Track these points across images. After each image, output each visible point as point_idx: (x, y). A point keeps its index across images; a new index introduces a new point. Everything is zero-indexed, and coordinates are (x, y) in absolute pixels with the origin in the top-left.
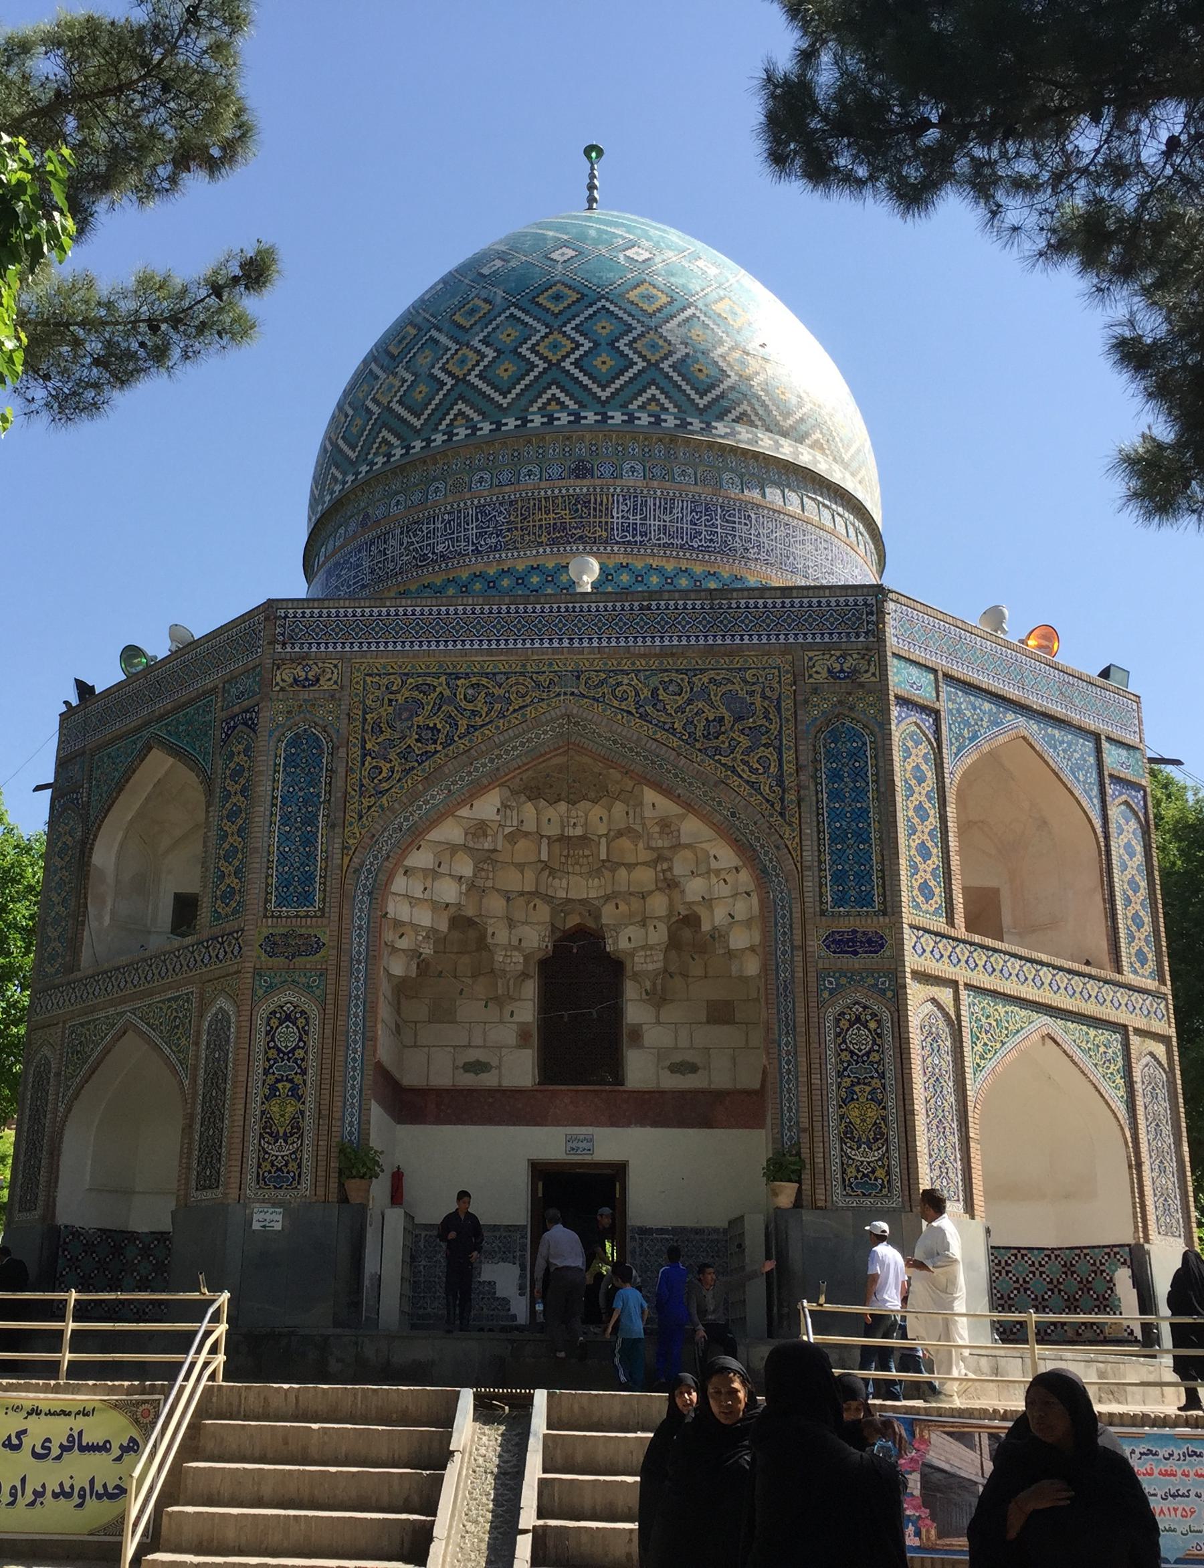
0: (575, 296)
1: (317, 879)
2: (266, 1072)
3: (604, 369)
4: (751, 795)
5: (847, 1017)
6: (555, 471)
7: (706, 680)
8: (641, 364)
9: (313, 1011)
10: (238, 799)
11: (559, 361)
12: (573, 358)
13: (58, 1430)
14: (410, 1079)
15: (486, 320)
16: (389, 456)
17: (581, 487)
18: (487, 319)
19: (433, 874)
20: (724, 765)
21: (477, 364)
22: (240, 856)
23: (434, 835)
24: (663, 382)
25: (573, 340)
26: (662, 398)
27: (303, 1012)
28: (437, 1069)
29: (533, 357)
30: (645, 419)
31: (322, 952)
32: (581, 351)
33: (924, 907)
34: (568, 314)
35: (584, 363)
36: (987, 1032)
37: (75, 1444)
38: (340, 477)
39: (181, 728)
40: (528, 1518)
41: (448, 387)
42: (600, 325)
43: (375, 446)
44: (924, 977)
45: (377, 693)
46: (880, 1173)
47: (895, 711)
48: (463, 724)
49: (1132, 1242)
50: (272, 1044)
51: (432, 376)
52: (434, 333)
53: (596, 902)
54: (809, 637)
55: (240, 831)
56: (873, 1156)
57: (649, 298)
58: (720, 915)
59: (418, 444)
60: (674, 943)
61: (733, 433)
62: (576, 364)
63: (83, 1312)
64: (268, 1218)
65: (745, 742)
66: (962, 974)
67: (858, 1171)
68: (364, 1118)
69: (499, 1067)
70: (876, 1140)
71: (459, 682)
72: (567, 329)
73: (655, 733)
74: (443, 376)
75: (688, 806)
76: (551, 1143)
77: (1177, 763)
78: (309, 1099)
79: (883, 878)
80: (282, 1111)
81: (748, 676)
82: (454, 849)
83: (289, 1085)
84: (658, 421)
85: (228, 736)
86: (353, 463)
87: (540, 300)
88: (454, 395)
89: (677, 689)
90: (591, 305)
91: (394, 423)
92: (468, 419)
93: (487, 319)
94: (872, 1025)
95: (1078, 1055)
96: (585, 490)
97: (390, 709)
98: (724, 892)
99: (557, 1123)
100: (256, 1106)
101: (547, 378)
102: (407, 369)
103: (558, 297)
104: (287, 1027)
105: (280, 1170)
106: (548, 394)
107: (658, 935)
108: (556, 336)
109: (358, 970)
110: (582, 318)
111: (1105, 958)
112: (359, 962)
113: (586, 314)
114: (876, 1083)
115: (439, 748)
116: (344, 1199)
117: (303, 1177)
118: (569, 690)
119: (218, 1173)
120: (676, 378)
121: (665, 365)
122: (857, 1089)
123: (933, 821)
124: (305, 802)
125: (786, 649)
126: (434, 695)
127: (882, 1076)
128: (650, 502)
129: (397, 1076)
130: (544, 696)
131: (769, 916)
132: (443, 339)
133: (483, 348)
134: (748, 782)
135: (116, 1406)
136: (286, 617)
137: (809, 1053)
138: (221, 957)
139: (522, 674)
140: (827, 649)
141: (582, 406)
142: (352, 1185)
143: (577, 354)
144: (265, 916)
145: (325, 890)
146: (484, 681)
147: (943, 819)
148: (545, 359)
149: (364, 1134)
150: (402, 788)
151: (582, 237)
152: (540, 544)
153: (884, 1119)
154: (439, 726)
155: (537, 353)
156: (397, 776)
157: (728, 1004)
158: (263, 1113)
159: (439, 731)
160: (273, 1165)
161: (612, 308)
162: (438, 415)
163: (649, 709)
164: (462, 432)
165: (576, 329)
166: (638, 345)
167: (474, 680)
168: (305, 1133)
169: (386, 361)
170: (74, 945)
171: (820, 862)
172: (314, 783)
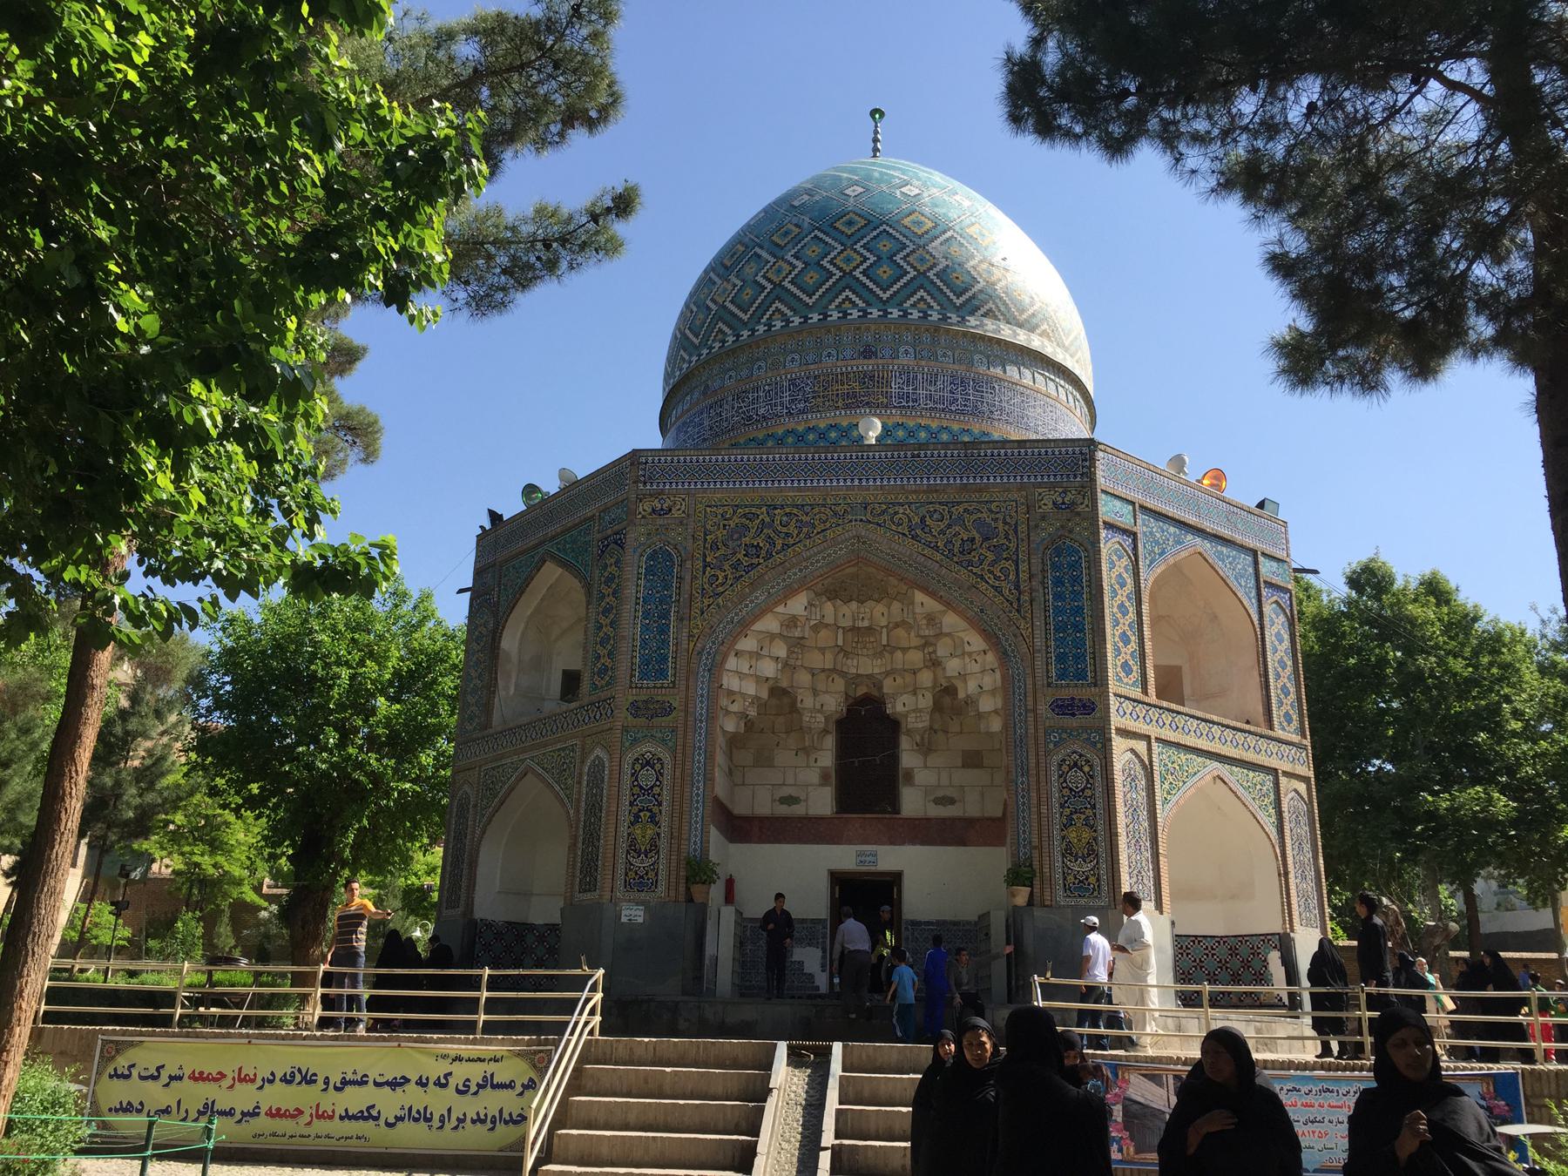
0: (863, 222)
2: (631, 804)
6: (848, 353)
8: (913, 273)
9: (667, 758)
13: (476, 1072)
14: (740, 809)
16: (724, 342)
17: (867, 365)
18: (797, 240)
19: (757, 655)
23: (758, 626)
26: (928, 298)
28: (759, 802)
29: (831, 268)
30: (915, 315)
34: (858, 235)
37: (488, 1083)
40: (828, 1139)
44: (1125, 733)
46: (1092, 880)
47: (1103, 533)
48: (779, 543)
51: (756, 282)
52: (757, 250)
56: (1087, 867)
57: (919, 223)
58: (972, 686)
59: (746, 333)
60: (937, 707)
61: (982, 325)
62: (864, 273)
63: (494, 984)
64: (633, 913)
65: (991, 556)
66: (1154, 731)
72: (857, 246)
74: (764, 282)
75: (948, 605)
76: (846, 857)
77: (1315, 572)
78: (664, 824)
80: (644, 833)
82: (772, 637)
84: (926, 316)
86: (696, 347)
87: (837, 225)
88: (772, 296)
91: (728, 317)
93: (797, 240)
94: (1086, 769)
95: (1241, 791)
98: (974, 668)
99: (850, 842)
100: (624, 830)
101: (842, 284)
103: (850, 223)
107: (926, 701)
111: (1261, 719)
114: (1089, 812)
116: (690, 899)
121: (931, 274)
123: (1132, 616)
124: (661, 602)
125: (1022, 487)
127: (1094, 807)
129: (730, 806)
131: (1009, 686)
132: (764, 254)
133: (795, 262)
135: (519, 1054)
137: (1038, 790)
140: (1052, 486)
142: (696, 889)
147: (1139, 614)
148: (841, 269)
149: (705, 850)
151: (869, 178)
157: (978, 753)
163: (919, 532)
164: (779, 324)
165: (863, 247)
166: (910, 259)
169: (722, 271)
172: (667, 587)
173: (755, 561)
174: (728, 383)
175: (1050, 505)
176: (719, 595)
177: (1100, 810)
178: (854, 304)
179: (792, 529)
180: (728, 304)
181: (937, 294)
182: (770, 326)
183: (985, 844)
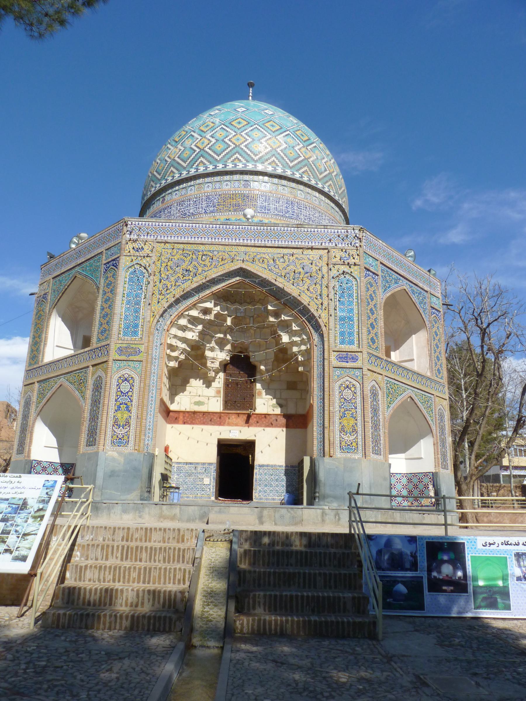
0: (246, 123)
1: (140, 326)
2: (116, 401)
5: (344, 386)
10: (109, 294)
11: (239, 145)
12: (244, 144)
15: (212, 129)
16: (173, 177)
18: (213, 129)
21: (209, 144)
22: (109, 316)
24: (278, 156)
25: (245, 138)
26: (277, 161)
27: (132, 378)
29: (229, 143)
31: (141, 354)
33: (372, 346)
34: (243, 129)
36: (391, 394)
38: (154, 185)
39: (88, 268)
41: (197, 152)
42: (255, 133)
43: (168, 173)
45: (167, 255)
46: (354, 444)
48: (200, 269)
49: (434, 471)
50: (119, 390)
51: (191, 148)
52: (193, 133)
55: (110, 306)
56: (352, 438)
59: (185, 173)
62: (246, 146)
67: (346, 443)
69: (208, 404)
72: (243, 134)
77: (452, 305)
78: (134, 410)
80: (122, 416)
83: (125, 406)
84: (275, 169)
85: (106, 270)
86: (159, 180)
87: (233, 123)
90: (252, 126)
92: (204, 164)
94: (353, 389)
96: (247, 192)
97: (172, 262)
100: (111, 414)
101: (235, 151)
102: (182, 145)
104: (126, 383)
105: (120, 439)
106: (235, 156)
108: (238, 136)
109: (155, 362)
110: (248, 130)
112: (155, 359)
113: (250, 129)
114: (353, 411)
115: (191, 278)
117: (130, 442)
119: (95, 440)
120: (282, 155)
124: (136, 297)
126: (189, 258)
128: (271, 198)
132: (196, 135)
133: (211, 139)
138: (100, 355)
139: (224, 252)
141: (247, 161)
143: (246, 143)
144: (118, 340)
145: (143, 331)
148: (234, 144)
152: (230, 211)
154: (191, 270)
155: (231, 141)
158: (114, 416)
159: (191, 271)
160: (118, 437)
161: (259, 128)
162: (193, 162)
163: (273, 268)
165: (246, 134)
173: (187, 278)
177: (359, 410)
179: (207, 263)
180: (176, 159)
182: (197, 169)
183: (294, 428)
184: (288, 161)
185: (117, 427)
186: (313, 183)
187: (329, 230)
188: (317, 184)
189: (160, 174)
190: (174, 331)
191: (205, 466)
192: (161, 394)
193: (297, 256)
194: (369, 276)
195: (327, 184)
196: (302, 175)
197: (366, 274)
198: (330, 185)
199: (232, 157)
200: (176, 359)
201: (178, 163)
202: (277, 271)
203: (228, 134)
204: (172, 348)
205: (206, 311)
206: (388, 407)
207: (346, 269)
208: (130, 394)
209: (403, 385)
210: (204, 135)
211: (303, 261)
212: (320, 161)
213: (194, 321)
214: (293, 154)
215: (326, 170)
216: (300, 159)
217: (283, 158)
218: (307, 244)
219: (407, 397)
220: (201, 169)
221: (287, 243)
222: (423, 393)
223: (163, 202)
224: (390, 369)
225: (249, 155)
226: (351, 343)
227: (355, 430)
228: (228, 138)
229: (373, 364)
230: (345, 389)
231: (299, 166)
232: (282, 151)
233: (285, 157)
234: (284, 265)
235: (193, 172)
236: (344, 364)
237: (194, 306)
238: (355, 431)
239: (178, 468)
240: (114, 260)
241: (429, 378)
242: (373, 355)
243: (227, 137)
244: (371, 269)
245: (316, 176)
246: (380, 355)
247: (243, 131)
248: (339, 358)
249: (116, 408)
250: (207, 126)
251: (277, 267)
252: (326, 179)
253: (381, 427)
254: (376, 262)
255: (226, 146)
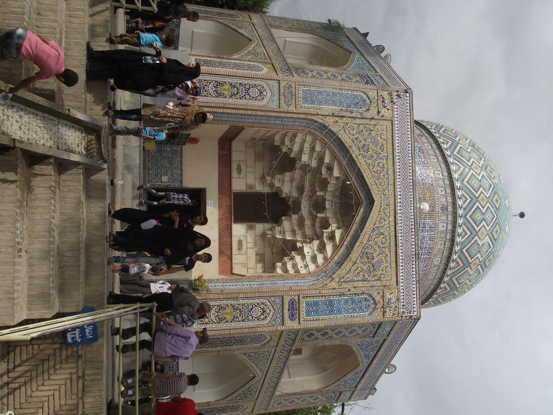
0: (497, 207)
2: (240, 84)
3: (476, 217)
4: (346, 270)
7: (387, 253)
8: (477, 229)
9: (265, 101)
11: (478, 201)
12: (480, 206)
14: (235, 145)
16: (443, 143)
18: (490, 177)
20: (357, 260)
21: (476, 173)
24: (471, 237)
25: (485, 206)
26: (466, 237)
27: (263, 99)
28: (238, 154)
29: (479, 192)
32: (482, 209)
33: (305, 335)
35: (478, 210)
38: (433, 128)
48: (369, 162)
52: (483, 159)
53: (300, 213)
54: (402, 291)
60: (285, 241)
62: (478, 207)
68: (223, 122)
69: (239, 178)
70: (219, 318)
71: (385, 161)
72: (488, 204)
73: (368, 234)
74: (471, 161)
78: (232, 101)
79: (316, 320)
81: (388, 269)
83: (236, 92)
84: (459, 235)
86: (438, 132)
87: (496, 195)
89: (383, 242)
91: (454, 145)
92: (459, 170)
93: (490, 177)
94: (262, 317)
97: (374, 135)
102: (471, 150)
105: (204, 88)
106: (468, 198)
112: (282, 121)
113: (493, 211)
114: (240, 318)
115: (361, 153)
118: (382, 202)
121: (477, 238)
122: (238, 311)
126: (380, 151)
127: (243, 321)
128: (433, 233)
129: (236, 139)
130: (380, 193)
132: (482, 162)
133: (481, 175)
134: (350, 269)
136: (407, 97)
139: (388, 184)
141: (465, 209)
143: (481, 207)
145: (308, 108)
146: (385, 170)
148: (479, 196)
150: (347, 138)
153: (227, 322)
154: (369, 153)
155: (481, 194)
156: (351, 136)
158: (225, 82)
160: (205, 86)
162: (459, 160)
163: (376, 232)
165: (488, 207)
166: (483, 228)
167: (386, 166)
168: (218, 99)
169: (472, 143)
170: (278, 27)
171: (322, 296)
174: (426, 145)
175: (390, 297)
176: (344, 131)
178: (464, 202)
180: (460, 145)
181: (468, 240)
182: (453, 164)
184: (467, 247)
185: (215, 85)
186: (449, 272)
187: (415, 286)
188: (447, 276)
189: (443, 132)
190: (309, 139)
191: (179, 176)
192: (248, 127)
193: (389, 255)
194: (374, 328)
195: (447, 286)
196: (455, 261)
197: (375, 325)
198: (446, 289)
199: (467, 194)
200: (283, 143)
201: (456, 147)
202: (374, 237)
203: (487, 190)
204: (292, 140)
205: (330, 169)
206: (245, 354)
207: (379, 306)
208: (248, 97)
209: (267, 368)
210: (484, 168)
211: (385, 262)
212: (467, 278)
213: (321, 160)
214: (474, 252)
215: (459, 284)
216: (469, 259)
217: (469, 242)
218: (401, 264)
219: (255, 373)
220: (453, 168)
221: (400, 245)
222: (259, 389)
223: (419, 135)
224: (282, 354)
225: (470, 210)
226: (308, 313)
227: (221, 321)
228: (483, 191)
229: (288, 336)
230: (262, 309)
231: (463, 258)
232: (476, 240)
233: (470, 244)
234: (379, 243)
235: (450, 160)
236: (286, 307)
237: (334, 157)
238: (220, 320)
239: (177, 151)
240: (372, 81)
241: (273, 394)
242: (296, 336)
243: (484, 190)
244: (380, 330)
245: (454, 274)
246: (296, 343)
247: (490, 205)
248: (293, 302)
249: (233, 84)
250: (491, 172)
251: (377, 236)
252: (452, 285)
253: (225, 347)
254: (386, 335)
255: (476, 189)
